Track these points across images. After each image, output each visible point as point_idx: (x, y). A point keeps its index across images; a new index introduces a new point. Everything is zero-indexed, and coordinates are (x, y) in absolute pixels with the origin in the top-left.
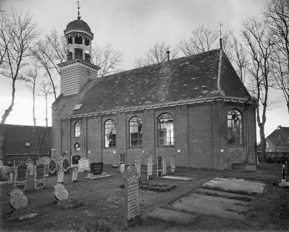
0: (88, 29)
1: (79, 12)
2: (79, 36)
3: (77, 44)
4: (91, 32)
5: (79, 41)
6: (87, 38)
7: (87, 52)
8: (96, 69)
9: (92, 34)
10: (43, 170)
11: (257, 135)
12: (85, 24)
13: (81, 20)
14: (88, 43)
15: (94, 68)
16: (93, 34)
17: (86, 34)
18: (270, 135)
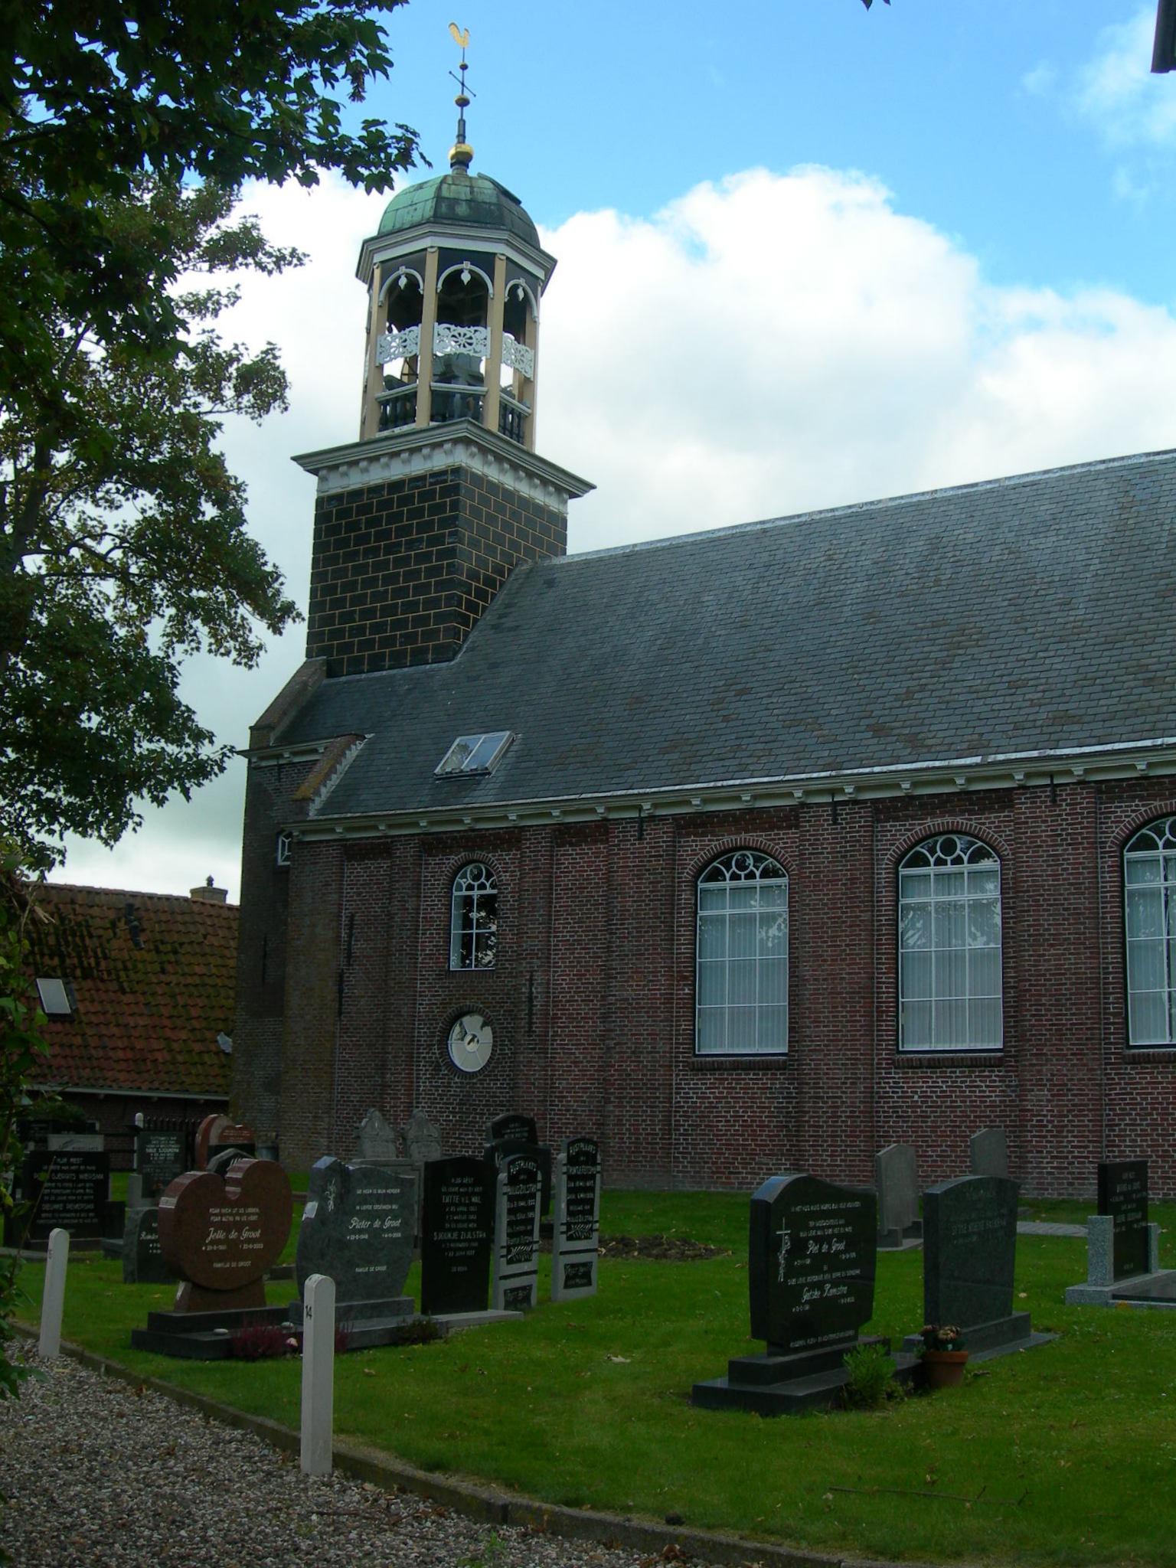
0: (526, 235)
1: (462, 123)
2: (466, 277)
3: (453, 327)
4: (544, 246)
5: (463, 305)
6: (515, 287)
8: (559, 490)
12: (505, 201)
14: (519, 319)
15: (553, 484)
18: (312, 574)
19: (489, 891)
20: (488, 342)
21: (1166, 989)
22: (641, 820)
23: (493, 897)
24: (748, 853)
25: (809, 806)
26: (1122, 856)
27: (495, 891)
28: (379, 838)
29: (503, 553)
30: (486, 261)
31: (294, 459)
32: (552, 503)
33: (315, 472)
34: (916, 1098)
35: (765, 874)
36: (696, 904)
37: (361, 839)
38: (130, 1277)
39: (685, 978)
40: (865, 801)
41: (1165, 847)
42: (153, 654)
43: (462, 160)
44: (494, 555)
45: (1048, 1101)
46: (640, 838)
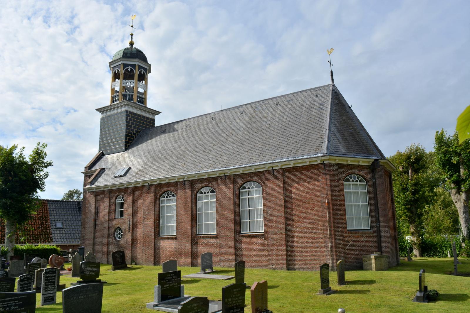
2: (129, 70)
3: (126, 80)
4: (148, 63)
5: (129, 76)
7: (141, 90)
8: (153, 114)
9: (150, 66)
10: (55, 276)
11: (306, 89)
13: (135, 48)
14: (142, 77)
16: (151, 65)
17: (145, 68)
19: (123, 201)
20: (123, 83)
21: (248, 220)
22: (149, 185)
23: (123, 202)
24: (169, 192)
25: (180, 181)
26: (239, 191)
27: (123, 201)
28: (102, 190)
29: (144, 126)
30: (134, 66)
31: (96, 110)
32: (151, 116)
33: (100, 112)
34: (200, 245)
35: (360, 181)
36: (160, 203)
37: (99, 191)
38: (101, 280)
39: (157, 219)
40: (190, 180)
41: (255, 188)
42: (14, 155)
43: (132, 44)
44: (138, 128)
45: (225, 246)
46: (149, 189)
